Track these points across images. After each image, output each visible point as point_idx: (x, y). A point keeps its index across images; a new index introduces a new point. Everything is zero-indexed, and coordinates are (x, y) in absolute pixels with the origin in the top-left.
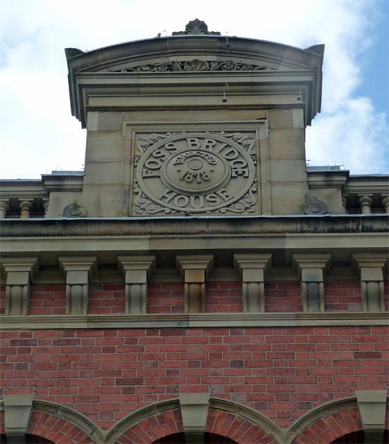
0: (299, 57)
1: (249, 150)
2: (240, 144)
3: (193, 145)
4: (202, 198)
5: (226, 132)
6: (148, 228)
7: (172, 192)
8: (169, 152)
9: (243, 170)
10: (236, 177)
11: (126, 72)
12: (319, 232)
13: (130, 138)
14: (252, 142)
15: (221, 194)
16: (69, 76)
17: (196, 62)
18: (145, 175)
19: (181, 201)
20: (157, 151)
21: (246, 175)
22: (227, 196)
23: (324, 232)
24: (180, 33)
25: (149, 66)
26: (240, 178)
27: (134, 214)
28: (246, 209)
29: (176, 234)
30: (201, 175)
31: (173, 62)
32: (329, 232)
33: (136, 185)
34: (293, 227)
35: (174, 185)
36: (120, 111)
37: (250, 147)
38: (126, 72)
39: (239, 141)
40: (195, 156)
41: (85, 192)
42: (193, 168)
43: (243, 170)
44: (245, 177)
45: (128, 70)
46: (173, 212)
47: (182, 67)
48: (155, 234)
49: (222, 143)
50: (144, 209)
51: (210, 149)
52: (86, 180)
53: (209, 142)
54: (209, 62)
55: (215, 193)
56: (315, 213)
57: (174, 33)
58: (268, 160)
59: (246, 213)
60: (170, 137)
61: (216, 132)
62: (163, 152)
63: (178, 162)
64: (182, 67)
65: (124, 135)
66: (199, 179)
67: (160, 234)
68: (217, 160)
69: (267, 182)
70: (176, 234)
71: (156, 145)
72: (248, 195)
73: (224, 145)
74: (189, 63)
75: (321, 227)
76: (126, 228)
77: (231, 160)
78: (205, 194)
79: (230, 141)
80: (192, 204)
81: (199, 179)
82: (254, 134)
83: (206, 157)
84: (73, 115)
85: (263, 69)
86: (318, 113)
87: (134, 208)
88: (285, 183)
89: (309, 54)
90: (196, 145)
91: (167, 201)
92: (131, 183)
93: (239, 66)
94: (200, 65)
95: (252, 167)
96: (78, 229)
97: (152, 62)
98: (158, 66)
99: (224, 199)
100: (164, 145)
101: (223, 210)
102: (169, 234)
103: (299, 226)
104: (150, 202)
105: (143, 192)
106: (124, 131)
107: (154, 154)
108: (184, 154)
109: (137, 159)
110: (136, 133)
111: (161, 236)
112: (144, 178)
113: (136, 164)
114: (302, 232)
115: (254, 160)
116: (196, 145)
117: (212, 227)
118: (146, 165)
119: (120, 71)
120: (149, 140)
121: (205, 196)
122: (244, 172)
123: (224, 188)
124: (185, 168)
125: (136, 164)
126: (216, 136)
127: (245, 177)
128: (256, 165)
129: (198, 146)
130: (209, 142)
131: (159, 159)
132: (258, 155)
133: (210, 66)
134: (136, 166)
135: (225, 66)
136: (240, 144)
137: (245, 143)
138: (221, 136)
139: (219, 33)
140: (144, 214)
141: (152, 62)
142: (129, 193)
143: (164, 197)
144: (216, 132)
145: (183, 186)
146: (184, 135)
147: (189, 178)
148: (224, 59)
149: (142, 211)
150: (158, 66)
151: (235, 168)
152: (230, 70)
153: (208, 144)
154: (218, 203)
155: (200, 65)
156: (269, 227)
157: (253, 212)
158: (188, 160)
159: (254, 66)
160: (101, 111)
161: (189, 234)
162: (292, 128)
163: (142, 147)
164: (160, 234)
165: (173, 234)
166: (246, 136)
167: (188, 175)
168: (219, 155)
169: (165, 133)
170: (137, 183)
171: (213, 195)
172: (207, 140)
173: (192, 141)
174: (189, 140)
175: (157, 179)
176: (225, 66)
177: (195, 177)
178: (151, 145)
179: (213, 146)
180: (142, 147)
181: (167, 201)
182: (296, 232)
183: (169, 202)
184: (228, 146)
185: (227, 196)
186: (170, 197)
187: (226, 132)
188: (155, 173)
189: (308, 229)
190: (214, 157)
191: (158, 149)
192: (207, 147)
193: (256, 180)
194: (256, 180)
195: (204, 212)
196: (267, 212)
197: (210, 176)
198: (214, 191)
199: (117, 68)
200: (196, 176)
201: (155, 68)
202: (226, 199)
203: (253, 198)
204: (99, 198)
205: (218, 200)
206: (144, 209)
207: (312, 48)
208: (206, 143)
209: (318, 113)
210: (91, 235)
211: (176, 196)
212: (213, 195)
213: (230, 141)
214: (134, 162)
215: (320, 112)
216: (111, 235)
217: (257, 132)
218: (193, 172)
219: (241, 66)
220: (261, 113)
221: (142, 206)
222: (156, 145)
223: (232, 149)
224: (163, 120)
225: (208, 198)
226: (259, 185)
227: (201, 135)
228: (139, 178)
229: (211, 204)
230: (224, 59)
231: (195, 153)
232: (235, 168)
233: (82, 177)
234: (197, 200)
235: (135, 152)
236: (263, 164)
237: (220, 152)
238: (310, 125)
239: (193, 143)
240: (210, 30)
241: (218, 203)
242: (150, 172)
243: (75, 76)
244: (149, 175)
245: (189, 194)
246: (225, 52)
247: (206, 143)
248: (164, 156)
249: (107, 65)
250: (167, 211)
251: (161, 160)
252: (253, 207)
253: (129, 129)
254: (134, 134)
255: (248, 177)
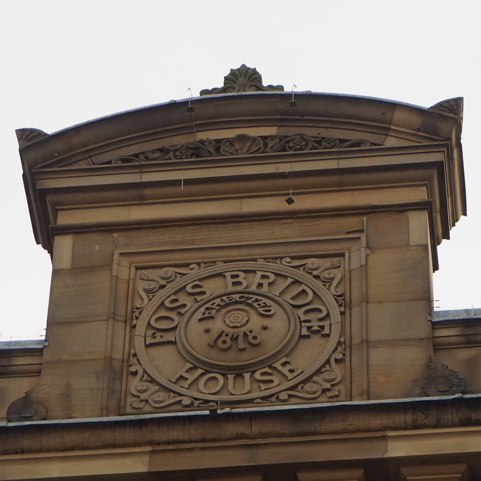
0: (416, 120)
1: (332, 288)
2: (317, 277)
3: (234, 284)
4: (247, 376)
5: (293, 258)
6: (147, 434)
7: (195, 368)
8: (192, 298)
9: (321, 323)
10: (307, 337)
11: (120, 164)
12: (446, 426)
13: (126, 277)
14: (338, 274)
15: (280, 368)
16: (24, 176)
17: (242, 138)
18: (149, 341)
19: (211, 383)
20: (173, 297)
21: (326, 331)
22: (291, 371)
23: (453, 425)
24: (214, 90)
25: (161, 150)
26: (316, 339)
27: (129, 410)
28: (325, 391)
29: (196, 441)
30: (245, 335)
31: (202, 142)
32: (463, 425)
33: (134, 360)
34: (399, 419)
35: (200, 357)
36: (111, 231)
37: (335, 282)
38: (120, 164)
39: (315, 273)
40: (237, 302)
41: (46, 378)
42: (232, 325)
43: (321, 323)
44: (325, 336)
45: (124, 160)
46: (196, 403)
47: (218, 150)
48: (159, 444)
49: (286, 277)
50: (147, 401)
51: (265, 289)
52: (47, 356)
53: (263, 277)
54: (264, 138)
55: (270, 367)
56: (443, 393)
57: (203, 92)
58: (364, 304)
59: (323, 398)
60: (195, 272)
61: (276, 259)
62: (183, 299)
63: (206, 315)
64: (218, 150)
65: (114, 274)
66: (241, 344)
67: (168, 443)
68: (275, 308)
69: (362, 341)
70: (196, 441)
71: (171, 288)
72: (327, 367)
73: (290, 280)
74: (230, 142)
75: (450, 416)
76: (108, 436)
77: (300, 307)
78: (251, 368)
79: (300, 274)
80: (231, 388)
81: (241, 344)
82: (341, 259)
83: (255, 305)
84: (38, 243)
85: (358, 144)
86: (462, 217)
87: (130, 399)
88: (394, 343)
89: (442, 117)
90: (240, 283)
91: (186, 384)
92: (126, 357)
93: (316, 142)
94: (248, 145)
95: (336, 317)
96: (26, 442)
97: (165, 143)
98: (176, 150)
99: (286, 377)
100: (184, 287)
101: (284, 396)
102: (183, 442)
103: (409, 418)
104: (157, 387)
105: (145, 372)
106: (115, 266)
107: (167, 303)
108: (218, 301)
109: (137, 314)
110: (137, 268)
111: (171, 447)
112: (147, 346)
113: (134, 322)
114: (415, 428)
115: (340, 306)
116: (240, 283)
117: (257, 428)
118: (153, 323)
119: (110, 162)
120: (159, 280)
121: (253, 372)
122: (322, 327)
123: (285, 356)
124: (217, 325)
125: (134, 322)
126: (277, 266)
127: (325, 336)
128: (342, 313)
129: (244, 285)
130: (263, 277)
131: (175, 313)
132: (347, 296)
133: (265, 145)
134: (134, 327)
135: (291, 145)
136: (317, 277)
137: (326, 275)
138: (282, 266)
139: (281, 88)
140: (147, 408)
141: (165, 143)
142: (122, 375)
143: (181, 377)
144: (276, 259)
145: (214, 357)
146: (219, 267)
147: (224, 342)
148: (291, 131)
149: (142, 405)
150: (176, 150)
151: (305, 321)
152: (301, 149)
153: (261, 281)
154: (275, 383)
155: (248, 145)
156: (356, 421)
157: (337, 396)
158: (224, 311)
159: (342, 141)
160: (76, 233)
161: (219, 440)
162: (408, 245)
163: (147, 291)
164: (168, 443)
165: (190, 442)
166: (327, 263)
167: (223, 338)
168: (280, 300)
169: (187, 265)
170: (135, 355)
171: (267, 370)
172: (259, 274)
173: (233, 277)
174: (228, 275)
175: (170, 349)
176: (291, 145)
177: (235, 339)
178: (162, 287)
179: (270, 284)
180: (147, 291)
181: (186, 384)
182: (405, 429)
183: (190, 385)
184: (296, 282)
185: (291, 371)
186: (191, 378)
187: (293, 258)
188: (169, 337)
189: (426, 421)
190: (269, 302)
191: (174, 293)
192: (260, 285)
193: (342, 340)
194: (342, 340)
195: (251, 401)
196: (361, 395)
197: (263, 336)
198: (269, 362)
199: (105, 157)
200: (238, 337)
201: (171, 154)
202: (290, 376)
203: (337, 372)
204: (68, 386)
205: (276, 379)
206: (147, 401)
207: (440, 105)
208: (257, 278)
209: (462, 217)
210: (49, 451)
211: (202, 375)
212: (267, 370)
213: (300, 274)
214: (132, 319)
215: (465, 214)
216: (83, 448)
217: (347, 255)
218: (231, 331)
219: (319, 143)
220: (352, 222)
221: (143, 396)
222: (171, 288)
223: (303, 287)
224: (182, 243)
225: (257, 376)
226: (348, 348)
227: (250, 265)
228: (139, 343)
229: (263, 386)
230: (291, 131)
231: (236, 297)
232: (305, 321)
233: (41, 350)
234: (239, 379)
235: (133, 301)
236: (356, 311)
237: (281, 293)
238: (448, 237)
239: (234, 280)
240: (265, 83)
241: (275, 383)
242: (158, 335)
243: (33, 175)
244: (158, 340)
245: (225, 371)
246: (74, 155)
247: (257, 278)
248: (184, 306)
249: (88, 154)
250: (186, 401)
251: (180, 314)
252: (337, 388)
253: (125, 262)
254: (133, 270)
255: (328, 336)
